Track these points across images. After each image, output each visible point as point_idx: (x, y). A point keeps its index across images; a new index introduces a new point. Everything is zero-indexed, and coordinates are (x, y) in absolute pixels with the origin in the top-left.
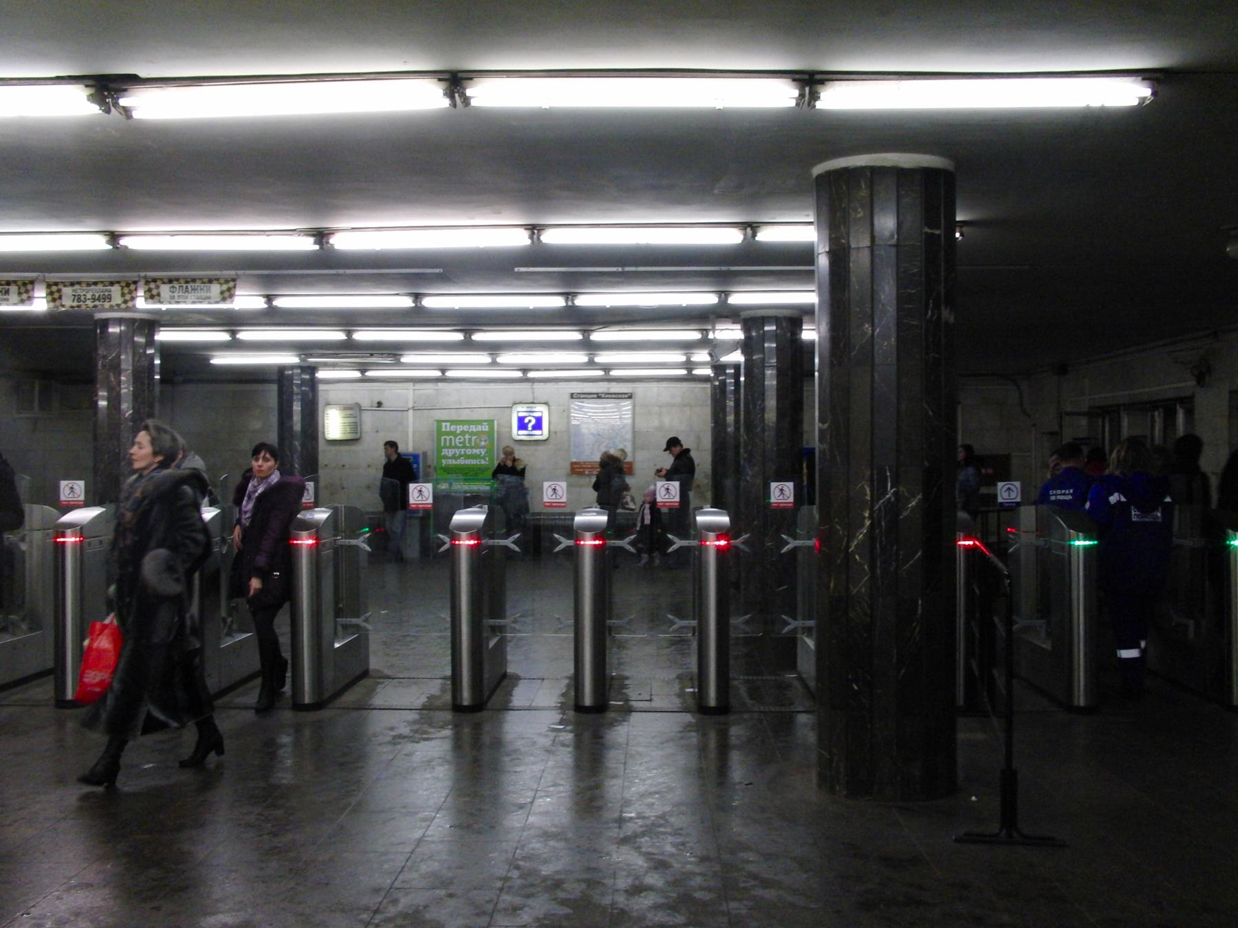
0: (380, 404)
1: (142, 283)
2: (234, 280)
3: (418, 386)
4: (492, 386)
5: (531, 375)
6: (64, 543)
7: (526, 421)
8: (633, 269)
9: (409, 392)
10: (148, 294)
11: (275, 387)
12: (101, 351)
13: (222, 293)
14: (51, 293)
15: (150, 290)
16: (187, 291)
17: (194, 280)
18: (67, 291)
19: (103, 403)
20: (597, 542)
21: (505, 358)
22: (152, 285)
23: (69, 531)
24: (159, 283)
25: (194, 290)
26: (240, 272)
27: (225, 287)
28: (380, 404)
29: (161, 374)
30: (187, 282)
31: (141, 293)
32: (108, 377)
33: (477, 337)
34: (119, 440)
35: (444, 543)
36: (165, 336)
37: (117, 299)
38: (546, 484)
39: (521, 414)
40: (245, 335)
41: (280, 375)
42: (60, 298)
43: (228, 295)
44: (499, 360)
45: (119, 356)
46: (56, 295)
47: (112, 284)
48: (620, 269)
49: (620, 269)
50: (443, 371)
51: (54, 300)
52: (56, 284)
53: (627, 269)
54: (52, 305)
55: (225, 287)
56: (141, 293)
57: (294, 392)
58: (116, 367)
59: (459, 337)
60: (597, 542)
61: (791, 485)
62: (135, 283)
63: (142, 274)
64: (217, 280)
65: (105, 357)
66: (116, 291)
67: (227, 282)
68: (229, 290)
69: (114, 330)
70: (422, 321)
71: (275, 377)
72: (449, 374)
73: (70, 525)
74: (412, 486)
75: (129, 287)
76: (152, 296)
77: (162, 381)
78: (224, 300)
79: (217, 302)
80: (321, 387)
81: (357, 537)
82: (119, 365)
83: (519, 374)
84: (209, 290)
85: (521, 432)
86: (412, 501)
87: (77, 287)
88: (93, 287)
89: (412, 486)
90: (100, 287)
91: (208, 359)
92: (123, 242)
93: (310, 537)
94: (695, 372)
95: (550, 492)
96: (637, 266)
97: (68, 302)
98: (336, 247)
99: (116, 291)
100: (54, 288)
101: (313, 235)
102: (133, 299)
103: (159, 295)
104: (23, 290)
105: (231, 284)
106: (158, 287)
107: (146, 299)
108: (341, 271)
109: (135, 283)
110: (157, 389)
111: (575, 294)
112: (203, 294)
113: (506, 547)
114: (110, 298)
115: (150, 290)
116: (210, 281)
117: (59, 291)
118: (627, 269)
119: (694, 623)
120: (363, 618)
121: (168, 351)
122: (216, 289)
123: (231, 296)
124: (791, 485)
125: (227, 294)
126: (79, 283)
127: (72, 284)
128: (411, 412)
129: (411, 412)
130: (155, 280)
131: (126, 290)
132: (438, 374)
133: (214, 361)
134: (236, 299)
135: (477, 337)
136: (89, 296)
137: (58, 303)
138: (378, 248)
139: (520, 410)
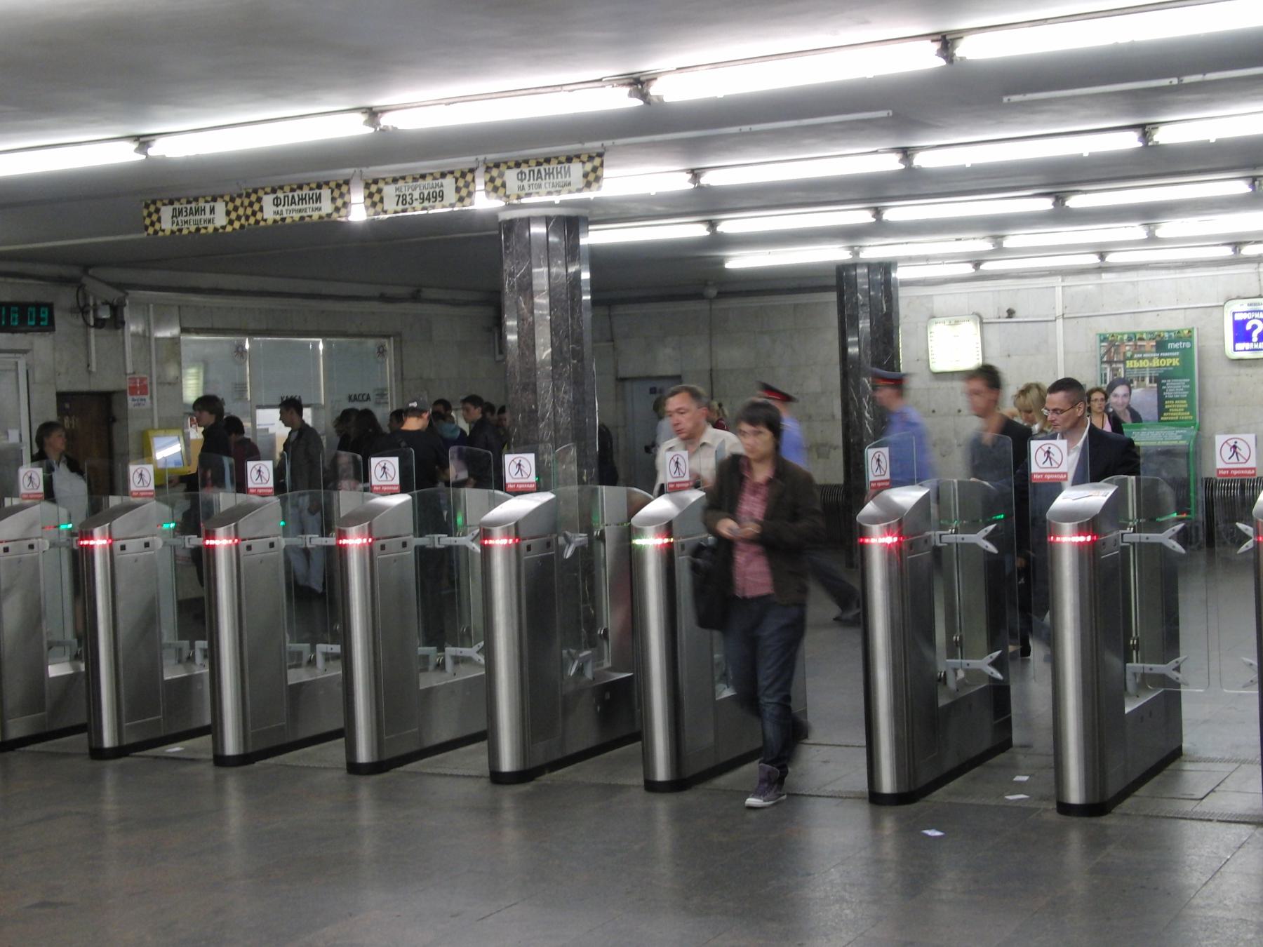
0: (1011, 313)
1: (481, 170)
2: (600, 155)
3: (1070, 281)
4: (1189, 273)
5: (1248, 251)
6: (214, 546)
7: (1248, 327)
8: (735, 129)
9: (1058, 293)
10: (490, 186)
11: (832, 297)
12: (508, 266)
13: (586, 175)
14: (370, 195)
15: (492, 180)
16: (539, 176)
17: (548, 161)
18: (389, 191)
19: (512, 338)
20: (1082, 539)
21: (1168, 228)
22: (495, 172)
23: (497, 531)
24: (503, 167)
25: (549, 174)
26: (608, 143)
27: (589, 166)
28: (1011, 313)
29: (593, 292)
30: (539, 164)
31: (480, 185)
32: (517, 303)
33: (1074, 202)
34: (535, 392)
35: (1247, 538)
36: (594, 237)
37: (451, 196)
38: (1219, 439)
39: (1239, 317)
40: (896, 213)
41: (841, 278)
42: (381, 200)
43: (592, 178)
44: (1159, 233)
45: (529, 273)
46: (376, 198)
47: (443, 175)
48: (1175, 81)
49: (1175, 81)
50: (977, 265)
51: (374, 205)
52: (376, 182)
53: (1187, 79)
54: (372, 211)
55: (589, 166)
56: (480, 185)
57: (863, 307)
58: (526, 288)
59: (1046, 204)
60: (1082, 539)
61: (395, 461)
62: (472, 171)
63: (481, 158)
64: (578, 157)
65: (512, 275)
66: (449, 184)
67: (591, 158)
68: (595, 170)
69: (538, 230)
70: (938, 189)
71: (833, 282)
72: (1111, 259)
73: (496, 523)
74: (250, 465)
75: (464, 177)
76: (495, 187)
77: (594, 302)
78: (588, 185)
79: (579, 190)
80: (903, 294)
81: (1160, 528)
82: (531, 284)
83: (1227, 252)
84: (568, 172)
85: (1240, 346)
86: (1035, 469)
87: (401, 183)
88: (421, 182)
89: (250, 465)
90: (429, 181)
91: (721, 262)
92: (386, 121)
93: (103, 538)
94: (984, 267)
95: (1227, 452)
96: (1204, 72)
97: (391, 209)
98: (667, 99)
99: (449, 184)
100: (374, 188)
101: (630, 84)
102: (470, 194)
103: (504, 185)
104: (337, 193)
105: (597, 161)
106: (501, 175)
107: (487, 193)
108: (746, 128)
109: (472, 171)
110: (587, 316)
111: (1155, 125)
112: (560, 180)
113: (1161, 546)
114: (441, 196)
115: (492, 180)
116: (569, 160)
117: (380, 191)
118: (1187, 79)
119: (337, 649)
120: (1173, 663)
121: (602, 260)
122: (577, 169)
123: (598, 179)
124: (395, 461)
125: (592, 177)
126: (403, 178)
127: (395, 180)
128: (1060, 322)
129: (1060, 322)
130: (497, 166)
131: (461, 183)
132: (1093, 260)
133: (729, 265)
134: (605, 183)
135: (1074, 202)
136: (416, 195)
137: (379, 208)
138: (720, 95)
139: (1239, 309)
